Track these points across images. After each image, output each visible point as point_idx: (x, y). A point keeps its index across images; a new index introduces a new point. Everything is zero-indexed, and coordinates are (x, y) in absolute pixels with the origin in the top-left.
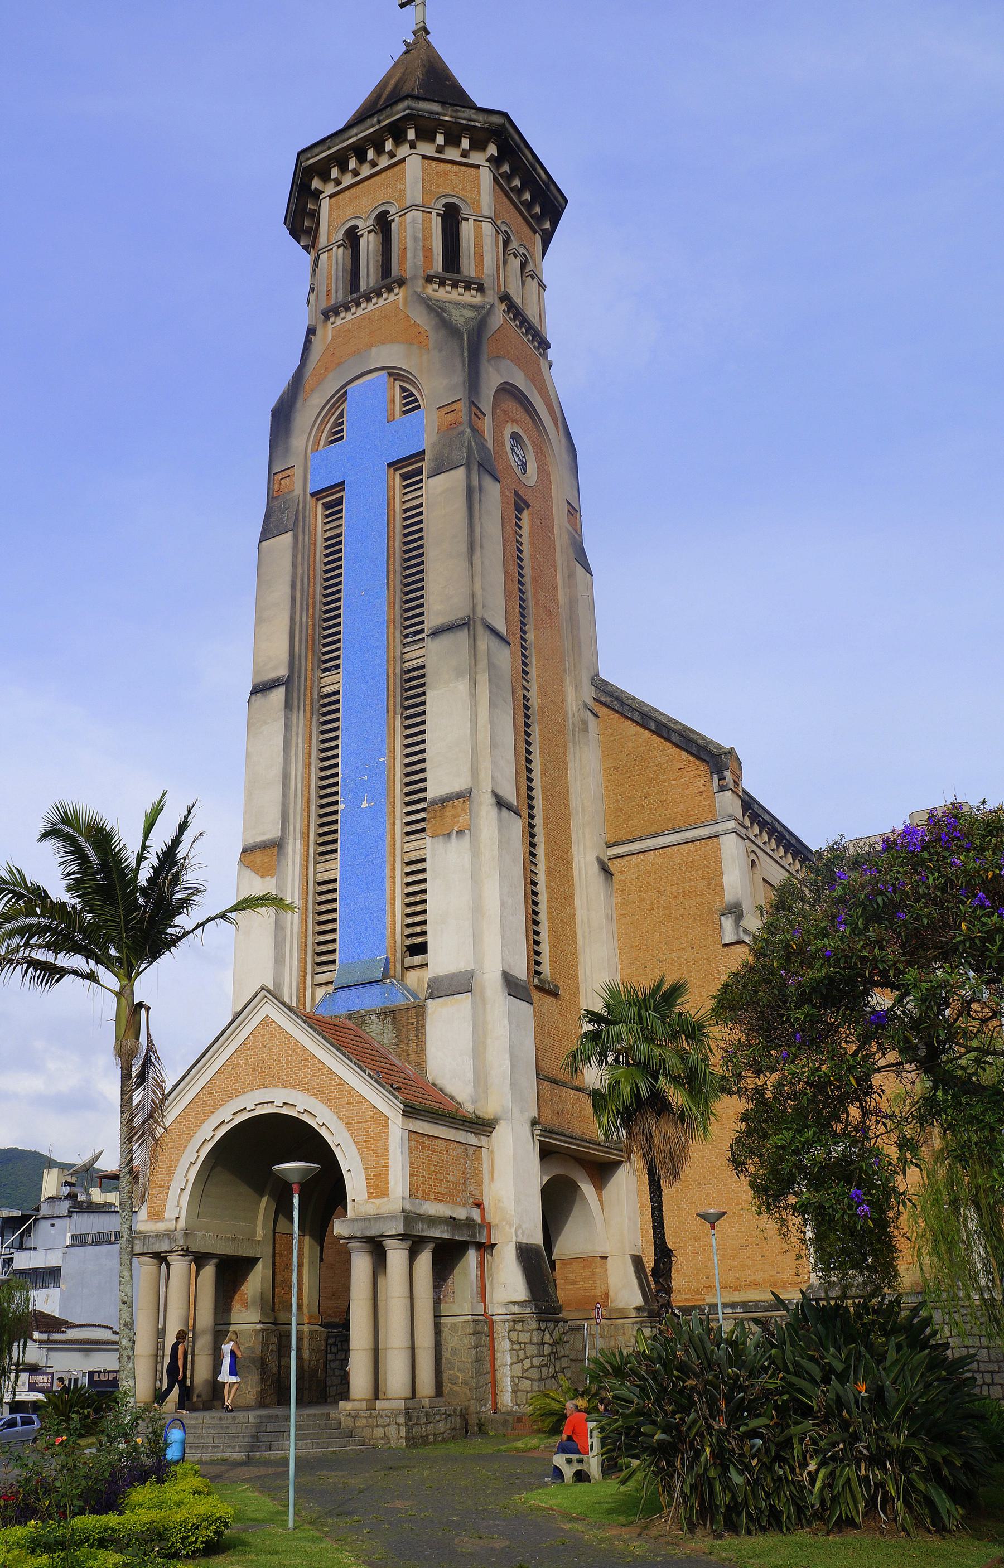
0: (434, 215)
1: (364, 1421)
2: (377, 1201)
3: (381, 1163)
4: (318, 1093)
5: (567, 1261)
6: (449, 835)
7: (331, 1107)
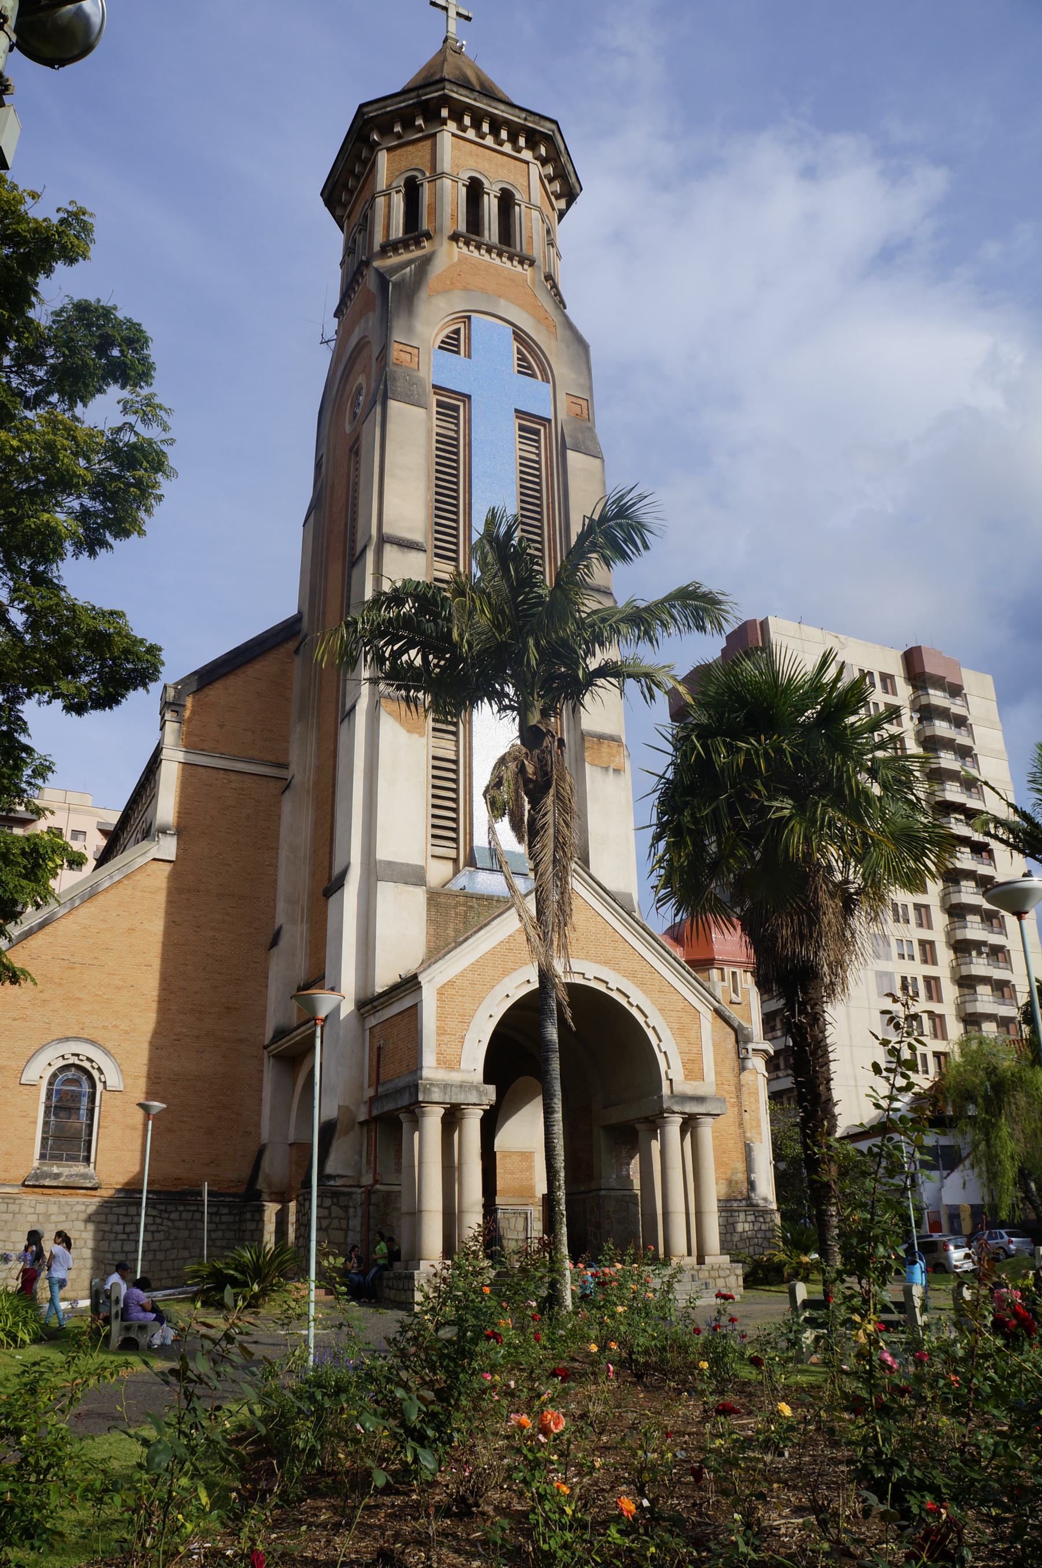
0: (460, 184)
1: (707, 1273)
2: (694, 1083)
3: (695, 1050)
4: (631, 975)
5: (508, 1154)
6: (607, 769)
7: (644, 991)
